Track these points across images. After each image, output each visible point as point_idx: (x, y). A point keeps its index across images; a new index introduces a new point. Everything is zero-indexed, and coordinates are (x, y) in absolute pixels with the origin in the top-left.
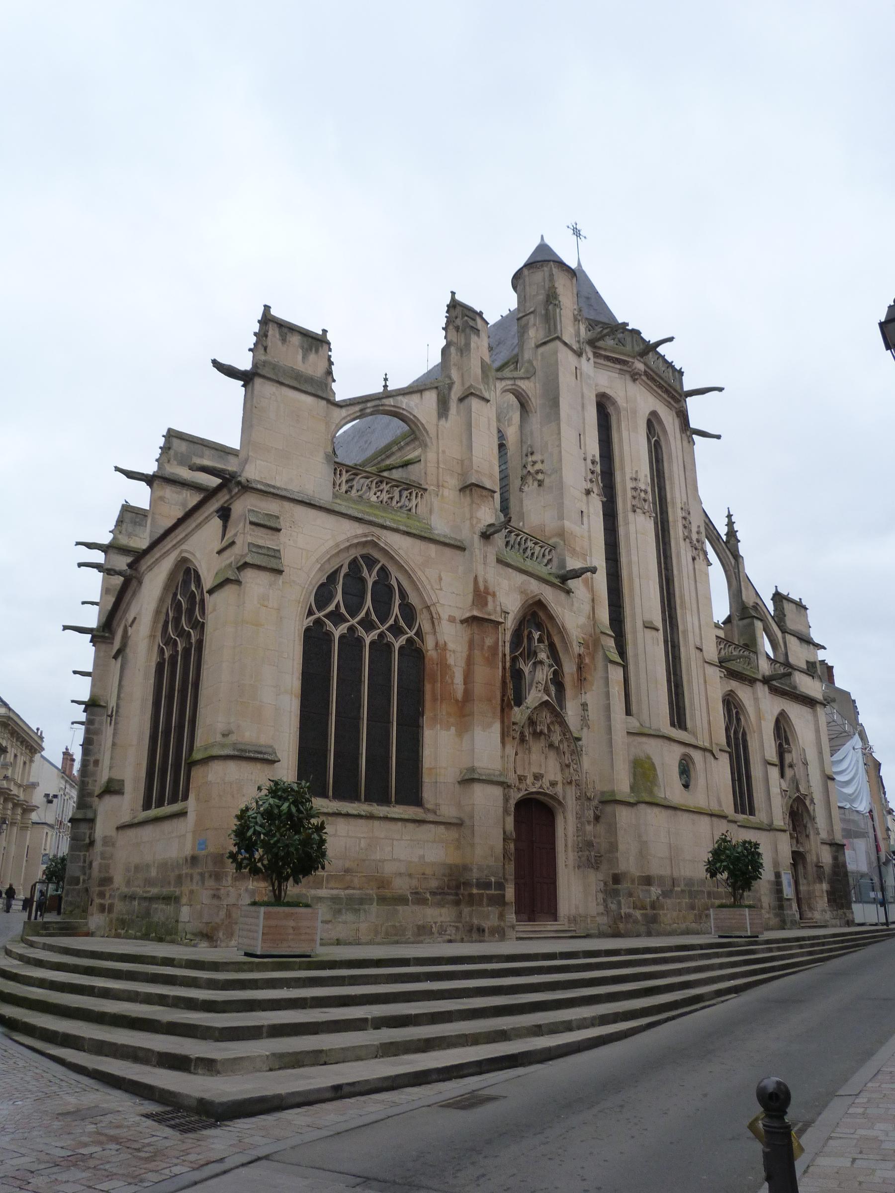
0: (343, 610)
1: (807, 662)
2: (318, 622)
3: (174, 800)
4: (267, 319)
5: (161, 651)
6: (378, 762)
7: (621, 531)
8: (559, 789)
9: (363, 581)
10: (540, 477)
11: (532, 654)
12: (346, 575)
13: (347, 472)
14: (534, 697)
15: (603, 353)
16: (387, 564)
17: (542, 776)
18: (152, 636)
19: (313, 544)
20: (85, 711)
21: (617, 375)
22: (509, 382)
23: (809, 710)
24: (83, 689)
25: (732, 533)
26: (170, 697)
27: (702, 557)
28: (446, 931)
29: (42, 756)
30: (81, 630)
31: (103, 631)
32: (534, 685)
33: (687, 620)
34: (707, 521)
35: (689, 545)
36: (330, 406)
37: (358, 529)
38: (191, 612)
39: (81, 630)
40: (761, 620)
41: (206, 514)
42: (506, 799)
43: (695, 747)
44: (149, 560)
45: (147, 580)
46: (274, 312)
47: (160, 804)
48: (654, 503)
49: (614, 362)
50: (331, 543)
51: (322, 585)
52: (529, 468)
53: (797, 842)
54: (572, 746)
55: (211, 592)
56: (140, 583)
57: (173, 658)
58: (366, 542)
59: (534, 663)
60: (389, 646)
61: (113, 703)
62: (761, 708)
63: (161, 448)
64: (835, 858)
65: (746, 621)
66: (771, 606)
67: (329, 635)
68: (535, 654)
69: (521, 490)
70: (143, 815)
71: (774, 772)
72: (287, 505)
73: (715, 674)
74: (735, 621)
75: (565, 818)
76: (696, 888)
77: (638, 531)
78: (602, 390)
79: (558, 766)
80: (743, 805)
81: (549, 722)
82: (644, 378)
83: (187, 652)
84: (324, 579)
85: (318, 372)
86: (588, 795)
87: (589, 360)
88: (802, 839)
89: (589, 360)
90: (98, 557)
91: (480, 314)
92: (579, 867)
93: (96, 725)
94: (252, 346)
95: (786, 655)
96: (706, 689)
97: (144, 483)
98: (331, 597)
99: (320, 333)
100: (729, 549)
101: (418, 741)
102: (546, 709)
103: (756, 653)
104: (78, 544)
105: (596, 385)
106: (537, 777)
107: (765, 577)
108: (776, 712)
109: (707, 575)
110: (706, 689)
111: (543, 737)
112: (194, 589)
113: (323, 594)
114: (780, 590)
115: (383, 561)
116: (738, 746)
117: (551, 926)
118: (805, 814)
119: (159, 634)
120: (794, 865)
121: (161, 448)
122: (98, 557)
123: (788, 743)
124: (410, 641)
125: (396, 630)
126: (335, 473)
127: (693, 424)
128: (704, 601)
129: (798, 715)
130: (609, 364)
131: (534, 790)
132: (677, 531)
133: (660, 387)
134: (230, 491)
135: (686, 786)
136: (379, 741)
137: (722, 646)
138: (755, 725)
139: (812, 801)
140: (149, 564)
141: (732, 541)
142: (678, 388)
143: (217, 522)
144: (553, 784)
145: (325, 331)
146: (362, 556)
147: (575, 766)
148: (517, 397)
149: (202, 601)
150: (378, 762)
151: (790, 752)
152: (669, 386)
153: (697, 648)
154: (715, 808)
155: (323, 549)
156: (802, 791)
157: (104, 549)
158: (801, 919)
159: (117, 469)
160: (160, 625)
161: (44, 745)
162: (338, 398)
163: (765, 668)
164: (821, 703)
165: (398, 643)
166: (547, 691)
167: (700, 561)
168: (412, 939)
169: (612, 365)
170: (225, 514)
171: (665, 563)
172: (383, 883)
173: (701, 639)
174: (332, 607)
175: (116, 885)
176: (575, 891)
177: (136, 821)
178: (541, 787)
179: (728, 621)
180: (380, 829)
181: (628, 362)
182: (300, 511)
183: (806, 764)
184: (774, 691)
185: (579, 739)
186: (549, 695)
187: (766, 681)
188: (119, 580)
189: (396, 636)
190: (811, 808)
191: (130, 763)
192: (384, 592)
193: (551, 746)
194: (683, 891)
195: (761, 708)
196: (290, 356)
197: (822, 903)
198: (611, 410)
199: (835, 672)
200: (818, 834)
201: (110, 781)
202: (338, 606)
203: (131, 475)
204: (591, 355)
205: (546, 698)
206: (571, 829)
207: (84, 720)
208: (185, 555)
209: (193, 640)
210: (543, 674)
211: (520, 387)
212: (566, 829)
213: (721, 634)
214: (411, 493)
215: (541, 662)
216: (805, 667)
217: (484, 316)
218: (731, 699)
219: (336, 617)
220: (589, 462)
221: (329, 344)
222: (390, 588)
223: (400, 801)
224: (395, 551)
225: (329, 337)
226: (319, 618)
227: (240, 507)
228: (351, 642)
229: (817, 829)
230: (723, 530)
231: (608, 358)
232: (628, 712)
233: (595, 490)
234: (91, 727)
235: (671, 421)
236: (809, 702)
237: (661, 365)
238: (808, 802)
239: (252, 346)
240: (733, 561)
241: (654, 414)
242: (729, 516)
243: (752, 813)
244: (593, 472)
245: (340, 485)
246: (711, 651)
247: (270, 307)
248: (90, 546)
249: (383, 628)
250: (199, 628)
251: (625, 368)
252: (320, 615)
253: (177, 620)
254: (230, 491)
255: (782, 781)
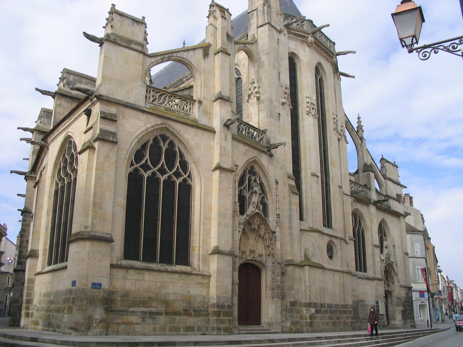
0: (149, 163)
1: (397, 194)
2: (136, 170)
3: (62, 261)
4: (113, 11)
5: (57, 184)
6: (166, 243)
7: (301, 124)
8: (264, 259)
9: (160, 148)
10: (258, 95)
11: (250, 187)
12: (151, 146)
13: (153, 91)
14: (251, 210)
15: (293, 31)
16: (173, 139)
17: (254, 251)
18: (53, 176)
19: (134, 128)
20: (22, 215)
21: (300, 43)
22: (242, 45)
23: (397, 219)
24: (21, 203)
25: (360, 127)
26: (61, 208)
27: (343, 139)
28: (201, 329)
29: (6, 238)
30: (20, 173)
31: (31, 174)
32: (251, 203)
33: (333, 171)
34: (347, 120)
35: (336, 133)
36: (145, 56)
37: (153, 121)
38: (71, 163)
39: (20, 173)
40: (374, 172)
41: (80, 113)
42: (234, 263)
43: (336, 237)
44: (52, 137)
45: (51, 147)
46: (117, 8)
47: (56, 263)
48: (318, 110)
49: (298, 36)
50: (144, 128)
51: (138, 150)
52: (252, 90)
53: (388, 286)
54: (271, 236)
55: (80, 153)
56: (48, 148)
57: (63, 187)
58: (162, 128)
59: (252, 193)
60: (174, 182)
61: (33, 211)
62: (372, 218)
63: (60, 78)
64: (407, 294)
65: (366, 173)
66: (379, 166)
67: (142, 177)
68: (252, 188)
69: (248, 102)
70: (48, 268)
71: (378, 251)
72: (121, 108)
73: (349, 200)
74: (361, 173)
75: (266, 273)
76: (333, 309)
77: (308, 125)
78: (292, 51)
79: (263, 246)
80: (360, 267)
81: (258, 223)
82: (314, 45)
83: (69, 184)
84: (139, 147)
85: (140, 39)
86: (279, 261)
87: (285, 35)
88: (391, 284)
89: (285, 35)
90: (29, 135)
91: (227, 10)
92: (273, 298)
93: (27, 222)
94: (105, 25)
95: (386, 191)
96: (342, 208)
97: (51, 97)
98: (143, 156)
99: (141, 18)
100: (357, 134)
101: (188, 232)
102: (257, 217)
103: (370, 189)
104: (18, 128)
105: (289, 48)
106: (252, 252)
107: (376, 151)
108: (380, 220)
109: (346, 148)
110: (342, 208)
111: (255, 231)
112: (73, 152)
113: (139, 155)
114: (384, 157)
115: (171, 138)
116: (359, 238)
117: (256, 327)
118: (392, 272)
119: (56, 175)
120: (386, 297)
121: (60, 78)
122: (29, 135)
123: (385, 236)
124: (185, 180)
125: (178, 174)
126: (147, 92)
127: (340, 70)
128: (342, 163)
129: (390, 221)
130: (296, 37)
131: (250, 258)
132: (330, 126)
133: (323, 50)
134: (91, 100)
135: (331, 257)
136: (167, 231)
137: (353, 185)
138: (369, 227)
139: (396, 266)
140: (52, 139)
141: (360, 131)
142: (332, 50)
143: (84, 117)
144: (261, 256)
145: (144, 18)
146: (160, 136)
147: (272, 247)
148: (246, 53)
149: (77, 158)
150: (166, 243)
151: (386, 240)
152: (325, 48)
153: (339, 186)
154: (345, 269)
155: (139, 132)
156: (392, 260)
157: (32, 131)
158: (388, 324)
159: (37, 89)
160: (57, 171)
161: (7, 232)
162: (149, 52)
163: (374, 197)
164: (403, 215)
165: (178, 181)
166: (257, 207)
167: (342, 141)
168: (183, 333)
169: (297, 38)
170: (88, 113)
171: (324, 141)
172: (167, 303)
173: (342, 182)
174: (143, 162)
175: (34, 304)
176: (270, 309)
177: (44, 271)
178: (253, 257)
179: (357, 172)
180: (166, 277)
181: (306, 37)
182: (128, 112)
183: (394, 247)
184: (380, 209)
185: (274, 232)
186: (259, 210)
187: (375, 203)
188: (38, 148)
189: (178, 178)
190: (396, 269)
191: (41, 241)
192: (171, 155)
193: (260, 236)
194: (326, 310)
195: (372, 218)
196: (127, 31)
197: (399, 317)
198: (296, 61)
199: (414, 200)
200: (399, 282)
201: (32, 251)
202: (146, 161)
203: (44, 93)
204: (286, 32)
205: (257, 211)
206: (269, 279)
207: (21, 219)
208: (69, 134)
209: (72, 178)
210: (255, 199)
211: (248, 48)
212: (267, 279)
213: (353, 179)
214: (187, 103)
215: (255, 192)
216: (396, 197)
217: (229, 11)
218: (356, 213)
219: (146, 167)
220: (284, 88)
221: (146, 24)
222: (175, 152)
223: (178, 263)
224: (178, 133)
225: (146, 21)
226: (137, 167)
227: (97, 109)
228: (153, 180)
229: (398, 279)
230: (355, 125)
231: (295, 34)
232: (301, 219)
233: (287, 103)
234: (25, 223)
235: (328, 67)
236: (397, 215)
237: (323, 39)
238: (394, 266)
239: (105, 25)
240: (360, 141)
241: (319, 64)
242: (359, 118)
243: (365, 271)
244: (286, 93)
245: (149, 98)
246: (347, 189)
247: (115, 5)
248: (26, 129)
249: (171, 173)
250: (75, 172)
251: (304, 40)
252: (136, 166)
253: (65, 168)
254: (91, 100)
255: (381, 255)
